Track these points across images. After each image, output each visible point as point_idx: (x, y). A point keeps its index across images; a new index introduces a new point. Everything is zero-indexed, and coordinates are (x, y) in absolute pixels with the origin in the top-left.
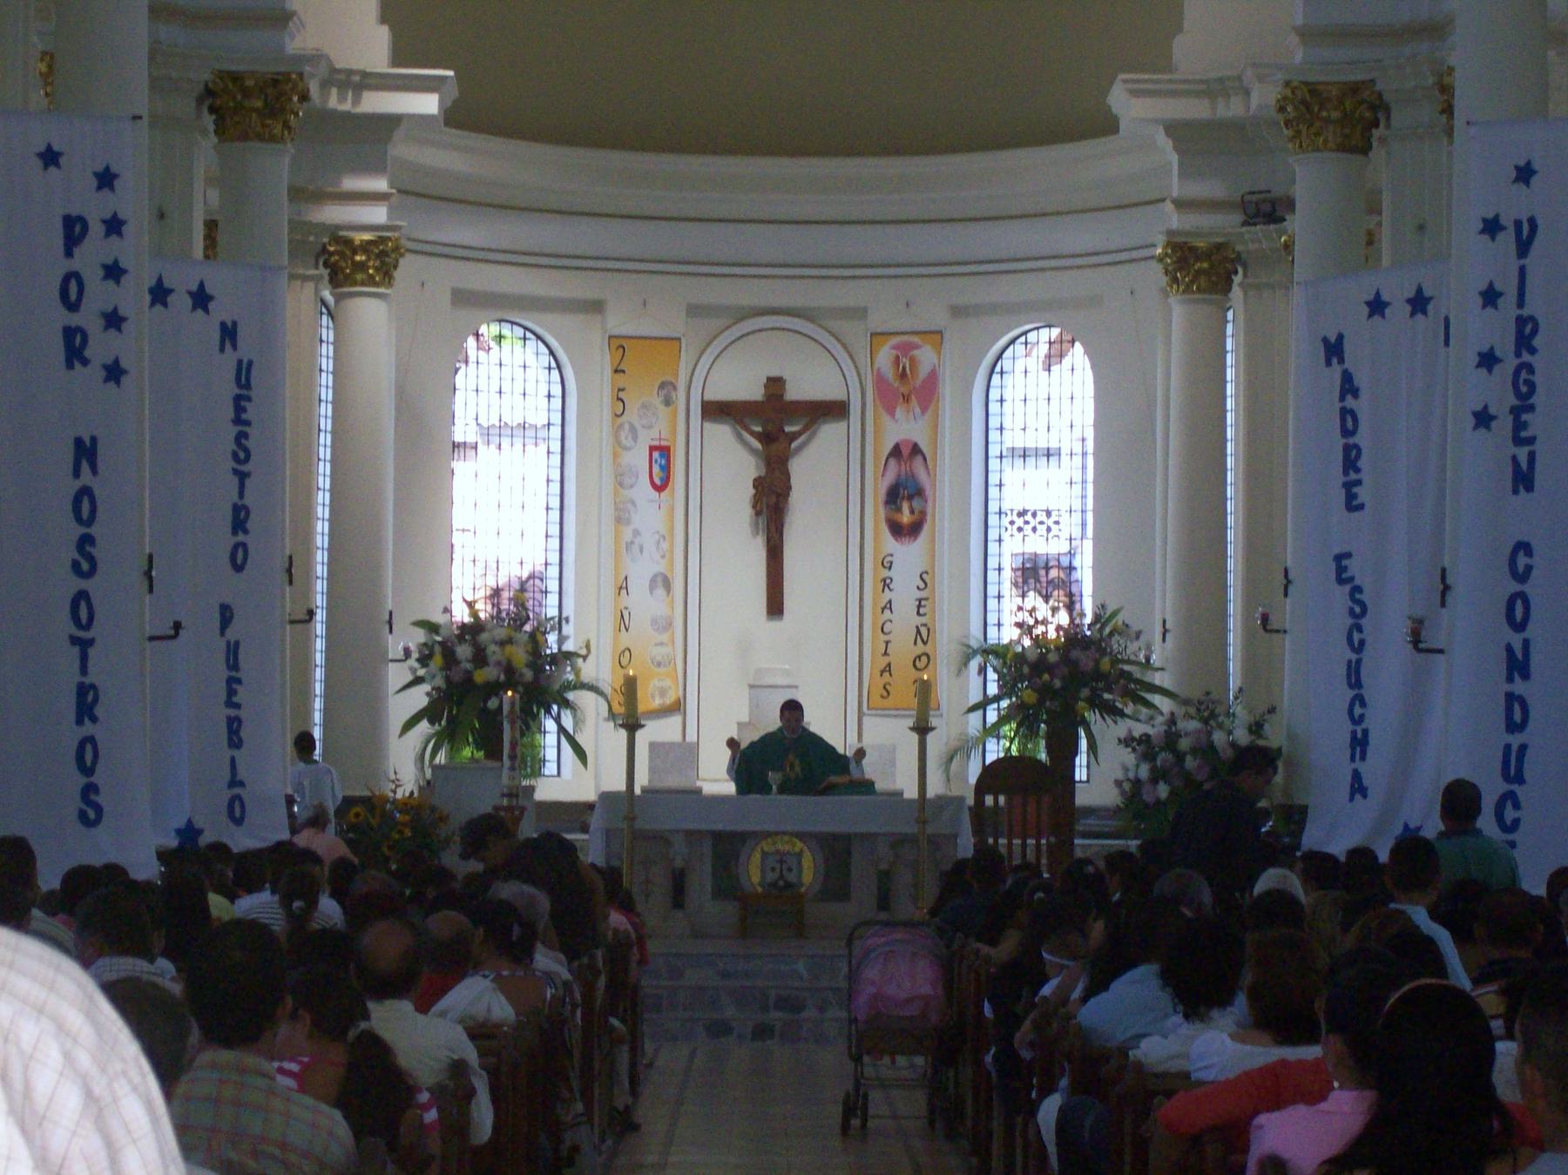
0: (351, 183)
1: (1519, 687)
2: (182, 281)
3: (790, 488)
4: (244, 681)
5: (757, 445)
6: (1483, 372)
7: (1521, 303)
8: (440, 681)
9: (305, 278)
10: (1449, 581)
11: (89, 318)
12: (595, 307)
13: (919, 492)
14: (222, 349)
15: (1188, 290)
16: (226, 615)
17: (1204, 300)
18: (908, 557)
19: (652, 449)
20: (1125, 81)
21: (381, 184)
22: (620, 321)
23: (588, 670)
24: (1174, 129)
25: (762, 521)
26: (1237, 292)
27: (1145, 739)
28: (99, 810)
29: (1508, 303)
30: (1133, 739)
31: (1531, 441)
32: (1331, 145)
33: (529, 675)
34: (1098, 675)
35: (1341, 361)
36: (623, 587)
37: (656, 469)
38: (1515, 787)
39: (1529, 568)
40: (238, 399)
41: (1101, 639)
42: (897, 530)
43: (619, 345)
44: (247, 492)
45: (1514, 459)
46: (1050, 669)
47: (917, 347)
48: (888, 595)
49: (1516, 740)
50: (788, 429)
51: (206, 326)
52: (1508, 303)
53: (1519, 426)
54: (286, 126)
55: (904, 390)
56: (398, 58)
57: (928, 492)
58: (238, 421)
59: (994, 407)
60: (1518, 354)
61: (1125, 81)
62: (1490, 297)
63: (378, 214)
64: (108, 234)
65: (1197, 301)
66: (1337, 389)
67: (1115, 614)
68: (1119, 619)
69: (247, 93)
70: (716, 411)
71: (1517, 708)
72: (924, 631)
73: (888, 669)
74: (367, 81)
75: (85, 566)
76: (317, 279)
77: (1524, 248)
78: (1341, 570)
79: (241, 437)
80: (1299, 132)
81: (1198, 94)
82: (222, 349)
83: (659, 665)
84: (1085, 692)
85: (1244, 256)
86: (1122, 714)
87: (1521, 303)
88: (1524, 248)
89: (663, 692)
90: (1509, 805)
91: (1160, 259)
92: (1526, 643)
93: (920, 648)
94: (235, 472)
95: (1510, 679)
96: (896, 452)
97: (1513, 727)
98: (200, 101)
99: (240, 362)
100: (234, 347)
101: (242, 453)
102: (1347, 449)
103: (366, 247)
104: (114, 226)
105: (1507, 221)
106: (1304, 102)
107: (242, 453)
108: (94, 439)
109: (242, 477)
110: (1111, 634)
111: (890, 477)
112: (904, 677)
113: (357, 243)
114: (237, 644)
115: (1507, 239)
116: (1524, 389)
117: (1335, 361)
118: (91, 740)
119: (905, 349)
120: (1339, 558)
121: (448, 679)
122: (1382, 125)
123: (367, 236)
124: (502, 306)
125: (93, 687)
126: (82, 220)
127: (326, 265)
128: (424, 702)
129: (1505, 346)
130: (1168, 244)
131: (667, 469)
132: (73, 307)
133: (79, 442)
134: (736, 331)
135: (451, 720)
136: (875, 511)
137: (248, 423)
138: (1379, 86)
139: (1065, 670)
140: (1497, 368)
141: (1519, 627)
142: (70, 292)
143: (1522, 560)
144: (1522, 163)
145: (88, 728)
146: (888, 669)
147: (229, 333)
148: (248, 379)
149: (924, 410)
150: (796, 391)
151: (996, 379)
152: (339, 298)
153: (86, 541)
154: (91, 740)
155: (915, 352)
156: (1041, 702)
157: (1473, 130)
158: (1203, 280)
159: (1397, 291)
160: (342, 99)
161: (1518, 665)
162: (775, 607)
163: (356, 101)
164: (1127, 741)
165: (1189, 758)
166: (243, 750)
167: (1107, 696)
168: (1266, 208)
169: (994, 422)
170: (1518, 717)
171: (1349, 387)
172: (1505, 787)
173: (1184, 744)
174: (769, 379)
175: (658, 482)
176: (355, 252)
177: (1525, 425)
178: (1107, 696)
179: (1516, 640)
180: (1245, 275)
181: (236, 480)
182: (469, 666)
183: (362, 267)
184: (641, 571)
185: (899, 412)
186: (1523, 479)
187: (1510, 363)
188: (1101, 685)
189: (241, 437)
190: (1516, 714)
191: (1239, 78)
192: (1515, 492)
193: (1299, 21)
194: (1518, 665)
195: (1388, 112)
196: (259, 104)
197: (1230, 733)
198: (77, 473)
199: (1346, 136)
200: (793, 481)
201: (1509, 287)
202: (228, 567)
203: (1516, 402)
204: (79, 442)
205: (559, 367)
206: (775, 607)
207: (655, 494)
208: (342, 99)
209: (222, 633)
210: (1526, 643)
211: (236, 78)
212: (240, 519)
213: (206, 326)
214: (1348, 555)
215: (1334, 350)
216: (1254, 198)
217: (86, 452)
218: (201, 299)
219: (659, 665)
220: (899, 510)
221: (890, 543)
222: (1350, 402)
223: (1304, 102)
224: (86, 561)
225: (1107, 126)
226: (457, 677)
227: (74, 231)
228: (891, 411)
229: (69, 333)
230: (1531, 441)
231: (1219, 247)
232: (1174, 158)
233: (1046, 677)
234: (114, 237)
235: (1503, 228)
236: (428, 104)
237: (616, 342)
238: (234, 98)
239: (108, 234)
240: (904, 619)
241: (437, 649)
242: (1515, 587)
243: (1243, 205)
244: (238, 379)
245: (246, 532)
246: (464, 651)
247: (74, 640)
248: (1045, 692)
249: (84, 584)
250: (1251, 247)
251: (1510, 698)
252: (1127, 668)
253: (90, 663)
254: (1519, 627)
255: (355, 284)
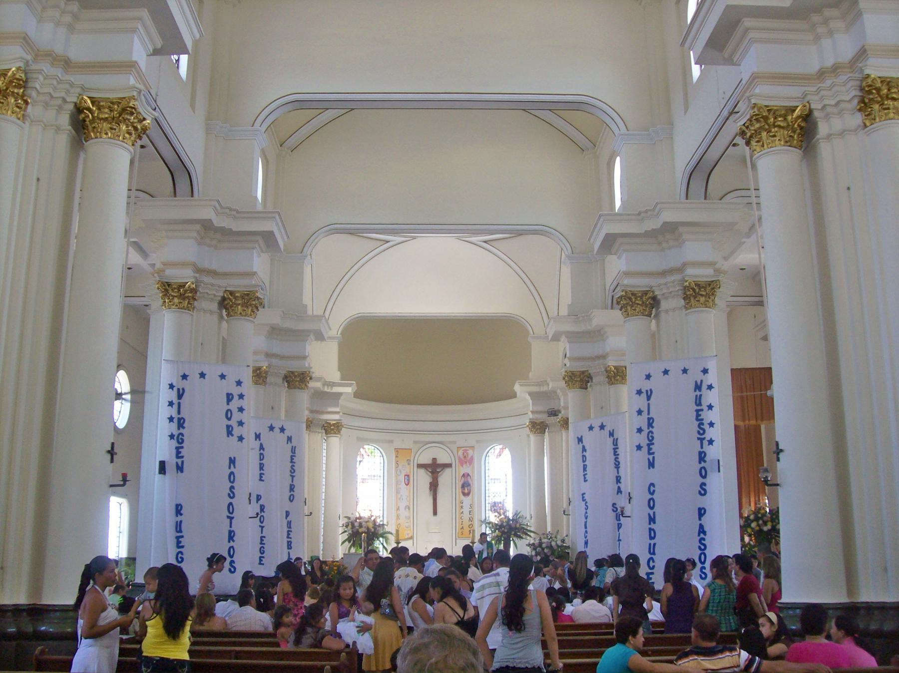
0: (330, 409)
1: (652, 526)
2: (277, 425)
3: (438, 485)
4: (293, 531)
5: (430, 474)
6: (638, 434)
7: (649, 414)
8: (350, 532)
9: (319, 433)
10: (631, 496)
11: (233, 423)
12: (391, 442)
13: (469, 485)
14: (287, 443)
15: (535, 433)
16: (288, 514)
17: (787, 150)
18: (467, 500)
19: (405, 475)
20: (519, 382)
21: (337, 410)
22: (398, 444)
23: (387, 529)
24: (530, 394)
25: (432, 492)
26: (547, 433)
27: (533, 544)
28: (235, 569)
29: (645, 414)
30: (530, 544)
31: (653, 453)
32: (577, 387)
33: (373, 530)
34: (516, 528)
35: (582, 443)
36: (398, 509)
37: (406, 480)
38: (653, 556)
39: (654, 491)
40: (292, 456)
41: (516, 519)
42: (464, 494)
43: (397, 450)
44: (294, 481)
45: (649, 459)
46: (504, 527)
47: (468, 450)
48: (462, 510)
49: (652, 542)
50: (438, 470)
51: (284, 437)
52: (645, 414)
53: (649, 449)
54: (306, 385)
55: (465, 460)
56: (342, 378)
57: (471, 485)
58: (292, 462)
59: (487, 464)
60: (648, 428)
61: (519, 382)
62: (640, 412)
63: (337, 417)
64: (239, 399)
65: (537, 436)
66: (581, 450)
67: (520, 513)
68: (520, 514)
69: (295, 376)
70: (420, 466)
71: (652, 532)
72: (471, 519)
73: (463, 528)
74: (333, 384)
75: (232, 495)
76: (322, 433)
77: (649, 398)
78: (583, 497)
79: (292, 467)
80: (569, 384)
81: (536, 385)
82: (287, 443)
83: (407, 527)
84: (513, 533)
85: (549, 425)
86: (522, 538)
87: (649, 414)
88: (649, 398)
89: (408, 534)
90: (651, 561)
91: (528, 426)
92: (654, 513)
93: (470, 523)
94: (291, 476)
95: (650, 524)
96: (464, 475)
97: (651, 538)
98: (283, 379)
99: (292, 447)
100: (291, 443)
101: (293, 470)
102: (584, 465)
103: (334, 425)
104: (241, 396)
105: (644, 390)
106: (570, 376)
107: (293, 470)
108: (234, 458)
109: (293, 477)
110: (519, 518)
111: (462, 482)
112: (466, 529)
113: (332, 423)
114: (291, 521)
115: (644, 395)
116: (650, 438)
117: (580, 443)
118: (232, 547)
119: (465, 451)
120: (583, 494)
121: (352, 531)
122: (590, 382)
123: (334, 422)
124: (369, 441)
125: (233, 531)
126: (231, 394)
127: (324, 429)
128: (347, 537)
129: (645, 427)
130: (530, 422)
131: (409, 480)
132: (229, 419)
133: (230, 458)
134: (425, 447)
135: (354, 541)
136: (459, 490)
137: (294, 463)
138: (589, 372)
139: (508, 527)
140: (642, 433)
141: (652, 508)
142: (228, 415)
143: (652, 488)
144: (647, 374)
145: (232, 544)
146: (463, 528)
147: (289, 439)
148: (295, 451)
149: (470, 465)
150: (440, 461)
151: (487, 458)
152: (327, 437)
153: (232, 488)
154: (232, 547)
155: (468, 451)
156: (502, 535)
157: (633, 365)
158: (539, 431)
159: (596, 425)
160: (328, 388)
161: (652, 520)
162: (435, 513)
163: (332, 389)
164: (529, 545)
165: (545, 549)
166: (292, 549)
167: (518, 534)
168: (553, 413)
169: (487, 468)
170: (653, 535)
171: (584, 450)
172: (650, 556)
173: (544, 546)
174: (433, 459)
175: (406, 483)
176: (331, 426)
177: (651, 449)
178: (518, 534)
179: (651, 512)
180: (549, 429)
181: (291, 478)
182: (357, 528)
183: (333, 429)
184: (402, 505)
185: (464, 466)
186: (651, 465)
187: (646, 431)
188: (517, 530)
189: (292, 467)
190: (652, 534)
191: (546, 381)
192: (649, 468)
193: (531, 410)
194: (652, 520)
195: (592, 378)
196: (298, 379)
197: (556, 542)
198: (230, 468)
199: (581, 385)
200: (439, 483)
201: (645, 410)
202: (288, 500)
203: (649, 442)
204: (230, 458)
205: (383, 456)
206: (435, 513)
207: (406, 486)
208: (328, 388)
209: (286, 518)
210: (654, 513)
211: (292, 373)
212: (292, 488)
213: (284, 437)
214: (584, 494)
215: (580, 440)
216: (550, 410)
217: (232, 461)
218: (282, 430)
219: (407, 527)
220: (465, 489)
221: (462, 497)
222: (584, 453)
223: (570, 376)
224: (232, 495)
225: (514, 395)
226: (355, 531)
227: (229, 398)
228: (462, 466)
229: (228, 427)
230: (653, 453)
231: (542, 422)
232: (531, 401)
233: (503, 529)
234: (241, 400)
235: (643, 392)
236: (349, 390)
237: (396, 450)
238: (231, 301)
239: (239, 399)
240: (466, 516)
241: (350, 523)
242: (651, 496)
243: (548, 412)
244: (292, 451)
245: (293, 491)
246: (356, 524)
247: (228, 517)
248: (503, 533)
249: (231, 500)
250: (550, 422)
251: (650, 529)
252: (523, 526)
253: (233, 524)
254: (652, 508)
255: (331, 434)
